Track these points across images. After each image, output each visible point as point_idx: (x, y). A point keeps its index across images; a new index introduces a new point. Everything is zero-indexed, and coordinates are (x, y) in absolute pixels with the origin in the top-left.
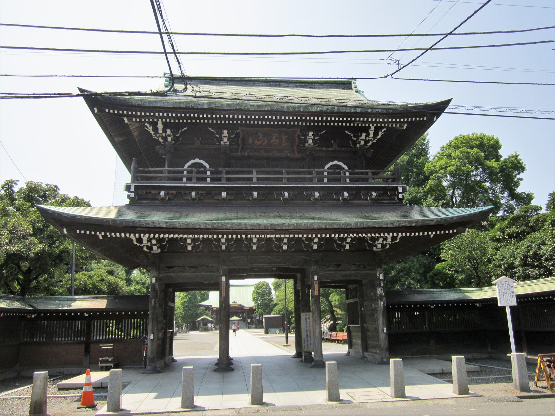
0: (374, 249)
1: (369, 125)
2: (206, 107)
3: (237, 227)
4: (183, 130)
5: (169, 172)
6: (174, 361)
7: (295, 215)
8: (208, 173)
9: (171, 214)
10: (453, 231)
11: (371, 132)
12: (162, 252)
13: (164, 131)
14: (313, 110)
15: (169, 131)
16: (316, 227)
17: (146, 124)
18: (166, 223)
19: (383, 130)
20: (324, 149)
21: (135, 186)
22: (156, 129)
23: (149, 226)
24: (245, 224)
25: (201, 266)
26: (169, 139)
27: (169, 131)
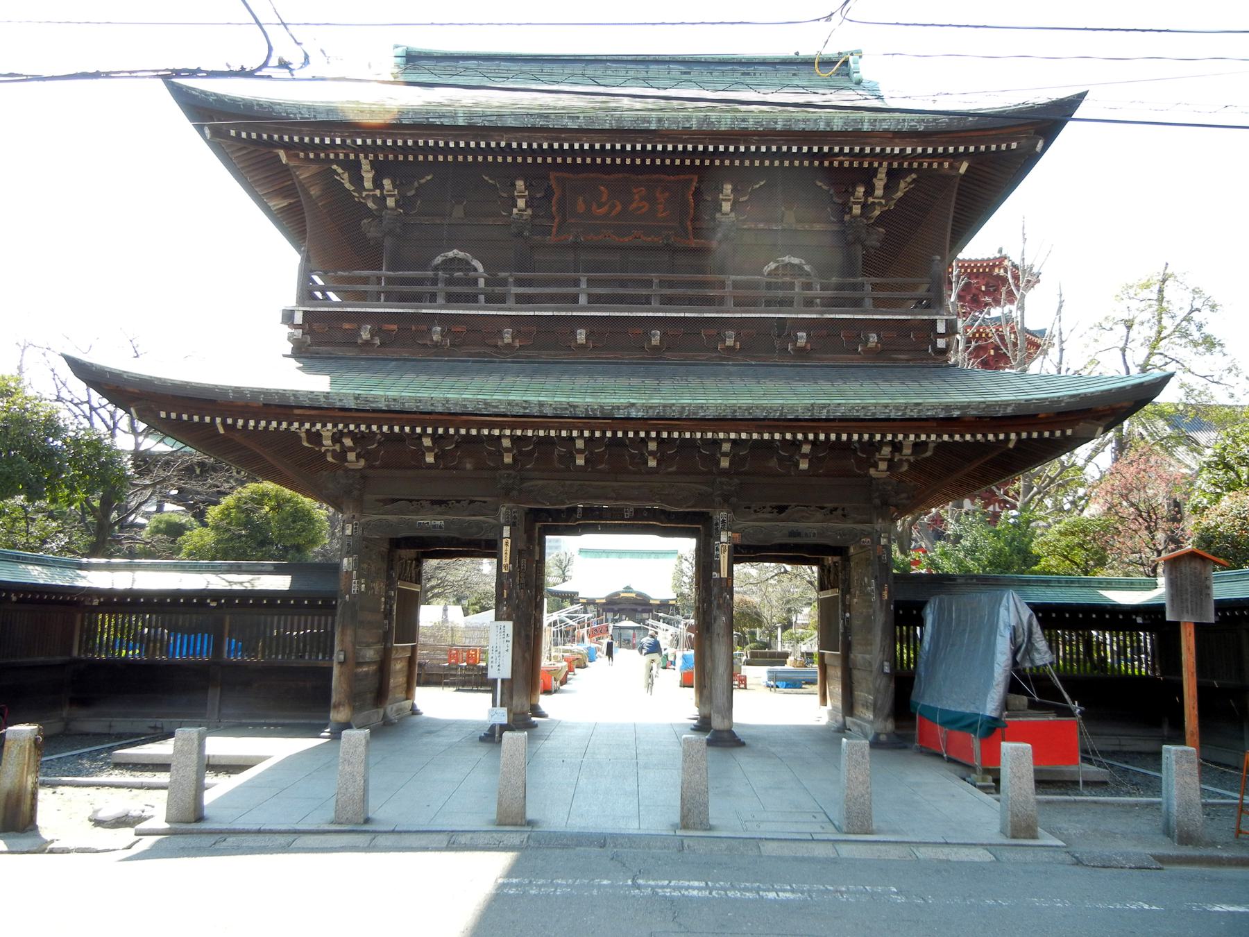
0: (872, 471)
1: (357, 156)
2: (461, 122)
3: (522, 411)
4: (423, 181)
5: (390, 281)
6: (414, 711)
7: (666, 385)
8: (481, 282)
9: (375, 379)
10: (1063, 432)
11: (880, 183)
12: (369, 466)
13: (377, 183)
14: (723, 128)
15: (387, 183)
16: (710, 414)
17: (334, 167)
18: (357, 398)
19: (909, 179)
20: (761, 226)
21: (305, 312)
22: (357, 180)
23: (316, 404)
24: (541, 404)
25: (458, 502)
26: (391, 202)
27: (387, 183)
